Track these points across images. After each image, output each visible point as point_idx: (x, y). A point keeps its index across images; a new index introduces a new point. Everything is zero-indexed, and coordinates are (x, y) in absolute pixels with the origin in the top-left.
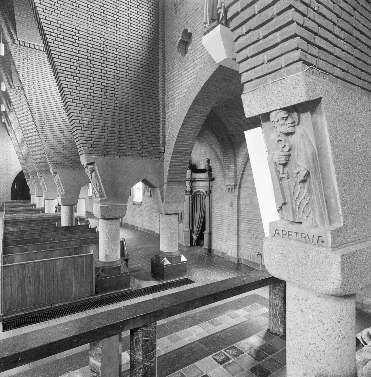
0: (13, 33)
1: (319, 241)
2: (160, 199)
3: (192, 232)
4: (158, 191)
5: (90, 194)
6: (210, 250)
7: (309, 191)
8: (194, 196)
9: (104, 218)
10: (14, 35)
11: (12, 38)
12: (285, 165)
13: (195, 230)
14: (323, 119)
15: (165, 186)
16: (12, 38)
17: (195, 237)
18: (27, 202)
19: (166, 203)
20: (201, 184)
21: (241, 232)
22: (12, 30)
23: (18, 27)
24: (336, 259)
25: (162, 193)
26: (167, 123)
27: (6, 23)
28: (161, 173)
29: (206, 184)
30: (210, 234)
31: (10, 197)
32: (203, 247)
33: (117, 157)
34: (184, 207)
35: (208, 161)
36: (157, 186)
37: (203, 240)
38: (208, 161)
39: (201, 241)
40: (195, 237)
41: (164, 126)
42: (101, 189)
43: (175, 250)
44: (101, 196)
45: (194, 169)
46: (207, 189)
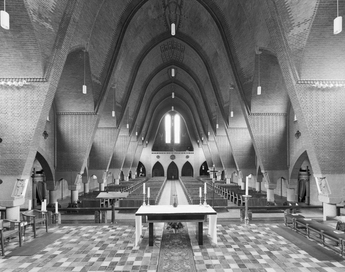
0: (228, 125)
1: (327, 196)
2: (288, 183)
3: (299, 196)
4: (287, 181)
5: (236, 175)
6: (309, 204)
7: (325, 189)
8: (300, 182)
9: (270, 189)
10: (228, 126)
11: (227, 127)
12: (321, 185)
13: (301, 195)
14: (326, 179)
15: (290, 179)
16: (227, 127)
17: (301, 198)
18: (208, 177)
19: (290, 185)
20: (304, 176)
21: (70, 118)
22: (227, 125)
23: (229, 123)
24: (329, 198)
25: (288, 181)
26: (290, 159)
27: (226, 123)
28: (288, 175)
29: (307, 176)
30: (309, 198)
31: (199, 175)
32: (305, 203)
33: (273, 171)
34: (296, 187)
35: (308, 167)
36: (286, 179)
37: (305, 200)
38: (308, 167)
39: (304, 201)
40: (301, 198)
41: (289, 159)
42: (268, 180)
43: (292, 201)
44: (269, 182)
45: (301, 170)
46: (307, 179)
